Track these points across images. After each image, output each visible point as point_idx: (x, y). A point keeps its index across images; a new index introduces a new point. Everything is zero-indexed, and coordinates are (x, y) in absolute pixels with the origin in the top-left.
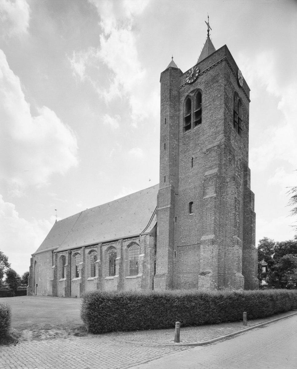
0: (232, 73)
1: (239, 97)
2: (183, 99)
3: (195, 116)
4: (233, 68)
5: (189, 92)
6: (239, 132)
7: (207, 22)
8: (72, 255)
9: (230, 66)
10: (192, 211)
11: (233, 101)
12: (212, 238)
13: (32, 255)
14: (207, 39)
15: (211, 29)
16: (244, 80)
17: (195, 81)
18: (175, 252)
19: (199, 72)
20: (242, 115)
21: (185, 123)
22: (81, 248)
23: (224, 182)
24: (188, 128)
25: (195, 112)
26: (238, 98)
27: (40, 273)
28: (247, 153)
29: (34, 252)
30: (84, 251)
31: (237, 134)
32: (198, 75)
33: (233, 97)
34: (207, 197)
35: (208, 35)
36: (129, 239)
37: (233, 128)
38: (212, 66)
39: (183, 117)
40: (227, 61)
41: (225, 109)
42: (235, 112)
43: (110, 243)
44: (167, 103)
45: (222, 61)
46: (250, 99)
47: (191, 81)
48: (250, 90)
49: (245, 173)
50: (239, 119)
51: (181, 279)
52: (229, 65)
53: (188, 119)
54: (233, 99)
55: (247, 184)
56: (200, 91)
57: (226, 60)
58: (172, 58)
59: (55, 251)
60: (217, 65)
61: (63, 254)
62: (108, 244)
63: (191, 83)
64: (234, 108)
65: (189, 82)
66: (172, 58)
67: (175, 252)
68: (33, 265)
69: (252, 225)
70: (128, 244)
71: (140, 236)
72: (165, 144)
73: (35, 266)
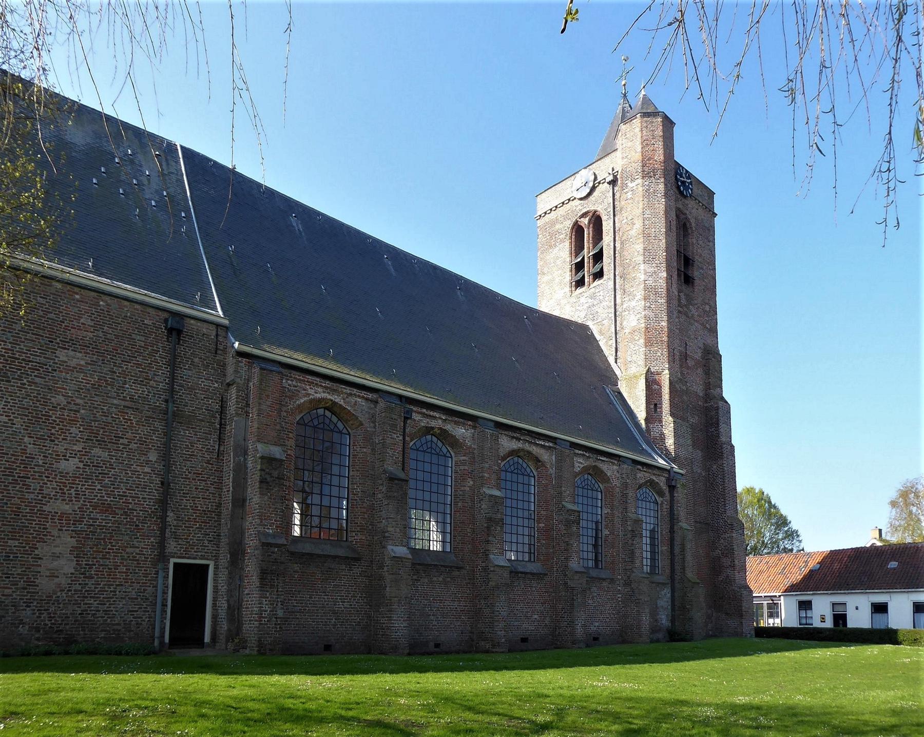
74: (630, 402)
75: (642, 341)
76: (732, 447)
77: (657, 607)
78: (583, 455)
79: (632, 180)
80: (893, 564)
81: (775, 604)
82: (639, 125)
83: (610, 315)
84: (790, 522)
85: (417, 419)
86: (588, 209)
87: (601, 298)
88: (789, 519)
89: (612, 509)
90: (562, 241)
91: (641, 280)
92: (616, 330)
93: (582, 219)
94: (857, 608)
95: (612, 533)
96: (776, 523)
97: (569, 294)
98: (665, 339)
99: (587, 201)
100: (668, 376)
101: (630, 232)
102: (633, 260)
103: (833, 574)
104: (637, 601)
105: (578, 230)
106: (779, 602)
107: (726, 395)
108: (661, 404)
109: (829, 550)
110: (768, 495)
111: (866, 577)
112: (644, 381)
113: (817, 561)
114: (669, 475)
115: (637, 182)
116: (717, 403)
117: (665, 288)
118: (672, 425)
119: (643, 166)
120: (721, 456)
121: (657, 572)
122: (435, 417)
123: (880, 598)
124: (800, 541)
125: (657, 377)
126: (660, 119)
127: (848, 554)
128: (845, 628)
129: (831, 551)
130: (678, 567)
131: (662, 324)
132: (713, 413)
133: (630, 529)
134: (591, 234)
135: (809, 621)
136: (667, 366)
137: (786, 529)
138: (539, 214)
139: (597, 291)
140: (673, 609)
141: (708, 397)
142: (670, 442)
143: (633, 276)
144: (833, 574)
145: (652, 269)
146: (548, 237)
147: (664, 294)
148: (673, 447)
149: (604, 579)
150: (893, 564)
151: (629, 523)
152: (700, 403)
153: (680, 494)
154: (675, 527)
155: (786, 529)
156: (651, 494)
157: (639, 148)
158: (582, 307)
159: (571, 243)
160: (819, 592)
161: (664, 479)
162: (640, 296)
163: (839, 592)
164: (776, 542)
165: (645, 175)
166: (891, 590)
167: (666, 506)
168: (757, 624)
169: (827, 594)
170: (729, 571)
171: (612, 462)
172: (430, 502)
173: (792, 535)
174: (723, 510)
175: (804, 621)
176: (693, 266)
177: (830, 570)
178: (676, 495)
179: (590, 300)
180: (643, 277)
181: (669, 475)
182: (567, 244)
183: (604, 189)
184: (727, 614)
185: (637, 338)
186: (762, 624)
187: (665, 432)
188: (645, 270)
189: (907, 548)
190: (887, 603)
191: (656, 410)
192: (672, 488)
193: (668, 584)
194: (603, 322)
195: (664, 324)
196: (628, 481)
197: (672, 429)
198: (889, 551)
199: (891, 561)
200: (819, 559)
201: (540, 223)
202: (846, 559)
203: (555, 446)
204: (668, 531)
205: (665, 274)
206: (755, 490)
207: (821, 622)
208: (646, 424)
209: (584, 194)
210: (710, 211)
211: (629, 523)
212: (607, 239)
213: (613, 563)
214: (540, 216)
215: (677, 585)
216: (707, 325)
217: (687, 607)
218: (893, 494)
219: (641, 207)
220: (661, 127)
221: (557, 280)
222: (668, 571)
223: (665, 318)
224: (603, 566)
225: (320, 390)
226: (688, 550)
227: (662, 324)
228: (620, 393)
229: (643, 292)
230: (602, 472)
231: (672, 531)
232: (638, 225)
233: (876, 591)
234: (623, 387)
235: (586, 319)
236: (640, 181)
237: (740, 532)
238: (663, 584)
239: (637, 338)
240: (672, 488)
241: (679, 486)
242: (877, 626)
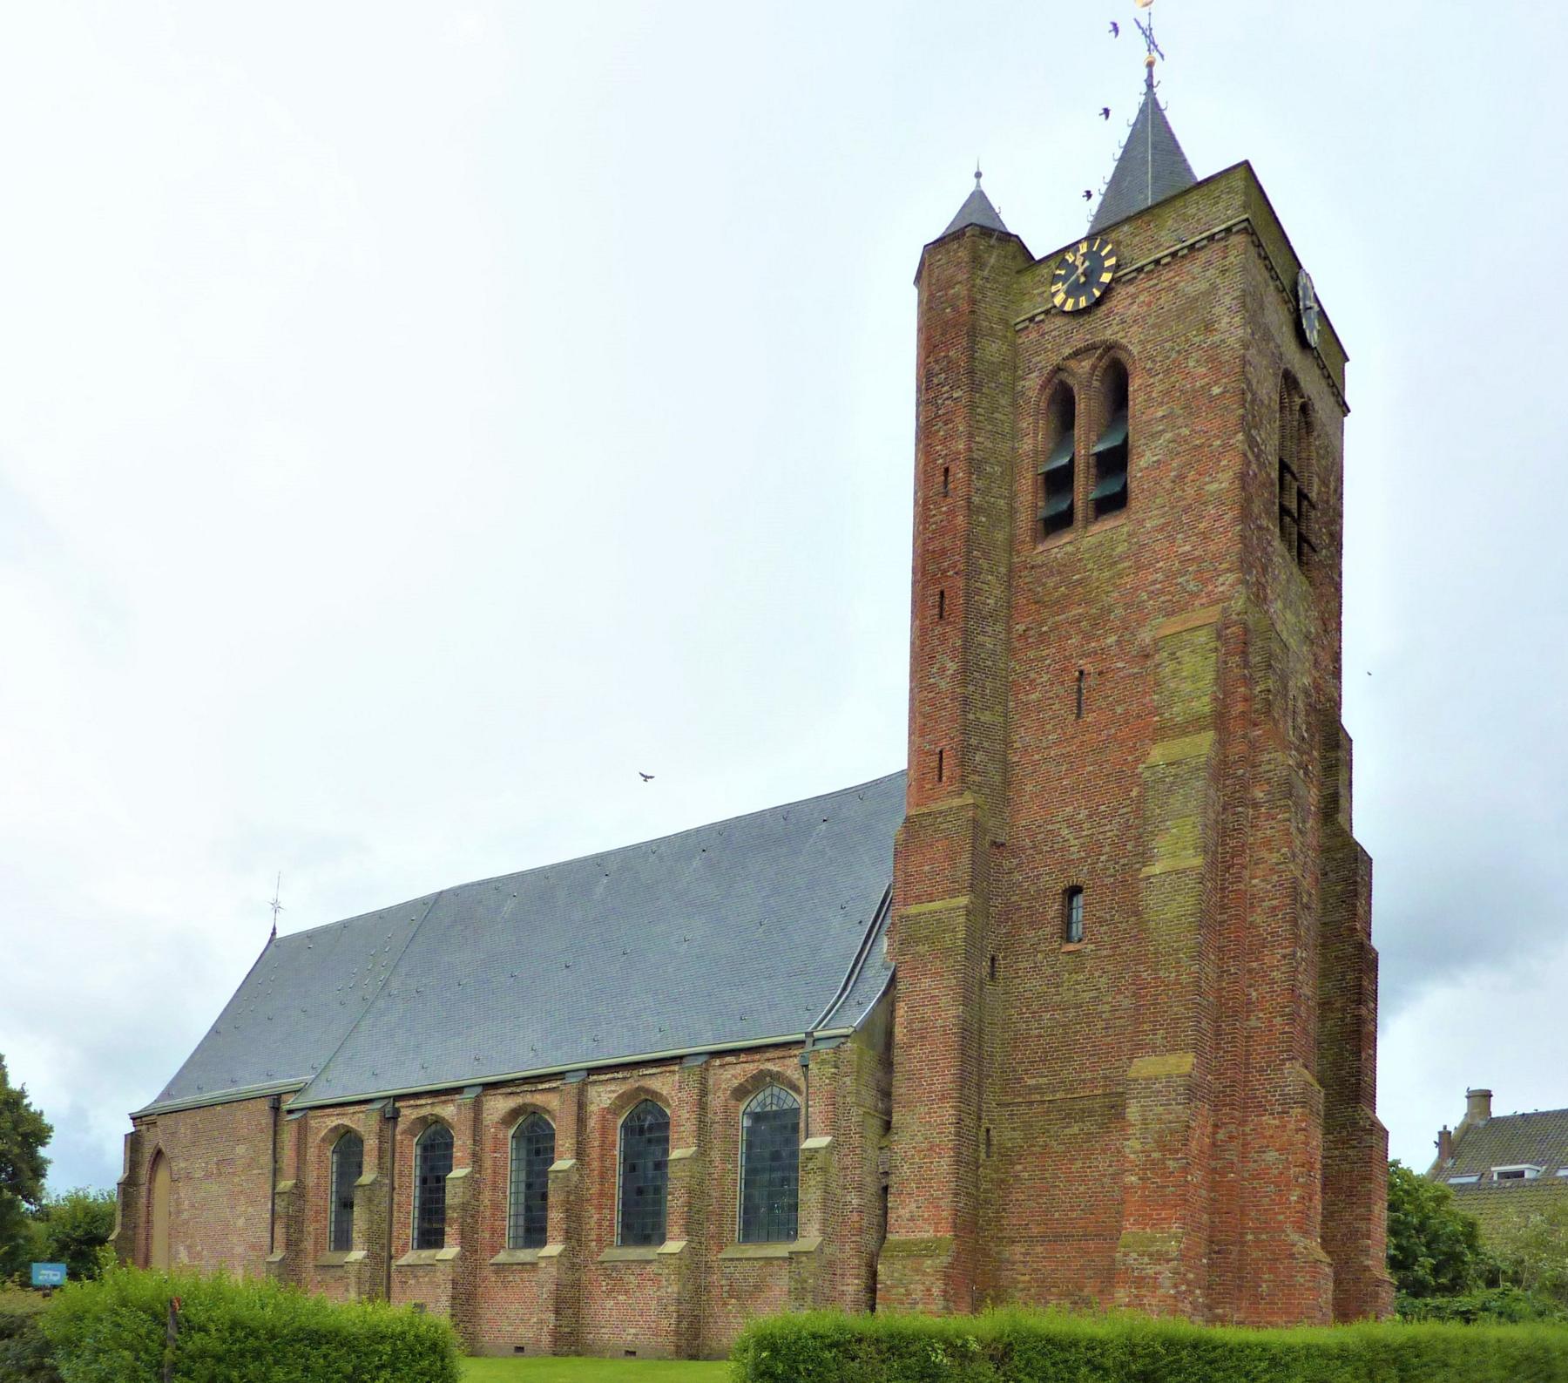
0: (1272, 288)
1: (1302, 397)
2: (1032, 384)
3: (1093, 471)
4: (1279, 262)
5: (1067, 351)
6: (1301, 561)
7: (1144, 24)
8: (401, 1127)
9: (1266, 258)
10: (1077, 930)
11: (1278, 415)
12: (1187, 1068)
13: (135, 1118)
14: (1142, 98)
15: (1162, 56)
16: (1322, 314)
17: (1099, 302)
18: (988, 1130)
19: (1118, 267)
20: (1315, 480)
21: (1041, 494)
22: (458, 1090)
23: (1242, 803)
24: (1058, 522)
25: (1099, 455)
26: (1298, 401)
27: (185, 1216)
28: (1337, 657)
29: (142, 1101)
30: (477, 1106)
31: (1295, 570)
32: (1113, 280)
33: (1276, 397)
34: (1157, 869)
35: (1150, 86)
36: (743, 1058)
37: (1277, 543)
38: (1182, 249)
39: (1035, 467)
40: (1253, 233)
41: (1245, 455)
42: (1284, 467)
43: (635, 1072)
44: (955, 395)
45: (1228, 230)
46: (1349, 398)
47: (1077, 303)
48: (1347, 359)
49: (1332, 755)
50: (1302, 496)
51: (1019, 1267)
52: (1263, 254)
53: (1058, 481)
54: (1277, 407)
55: (1336, 810)
56: (1122, 356)
57: (1249, 230)
58: (978, 175)
59: (289, 1103)
60: (1205, 246)
61: (346, 1121)
62: (620, 1075)
63: (1077, 313)
64: (1282, 446)
65: (1068, 307)
66: (978, 175)
67: (988, 1130)
68: (144, 1172)
69: (1364, 1011)
70: (736, 1083)
71: (809, 1041)
72: (942, 593)
73: (152, 1180)
85: (407, 1113)
122: (422, 1105)
171: (670, 1072)
206: (44, 1144)
225: (334, 1118)
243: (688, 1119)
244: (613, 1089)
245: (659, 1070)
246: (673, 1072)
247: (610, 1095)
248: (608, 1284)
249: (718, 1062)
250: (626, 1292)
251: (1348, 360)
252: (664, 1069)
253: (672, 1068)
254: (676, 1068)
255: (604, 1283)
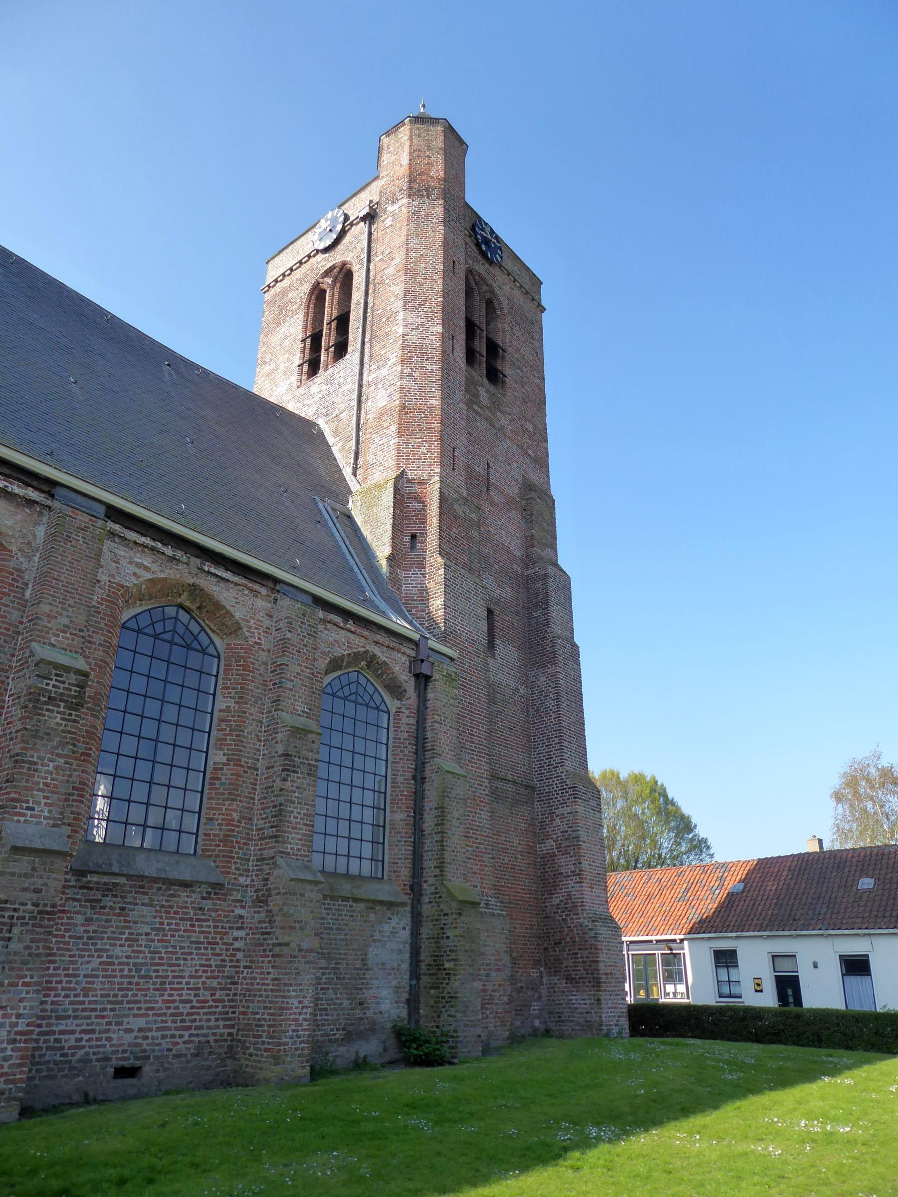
36: (350, 625)
62: (169, 551)
74: (366, 532)
75: (394, 428)
76: (575, 648)
77: (365, 967)
78: (153, 549)
79: (393, 202)
80: (866, 883)
81: (675, 954)
82: (408, 132)
83: (352, 404)
84: (695, 826)
86: (334, 262)
87: (341, 380)
88: (694, 820)
89: (241, 700)
90: (294, 313)
91: (398, 335)
92: (358, 424)
93: (325, 279)
94: (815, 966)
95: (234, 760)
96: (677, 827)
97: (295, 384)
98: (437, 426)
99: (331, 254)
100: (438, 486)
101: (386, 272)
102: (388, 309)
103: (767, 900)
104: (277, 950)
105: (318, 294)
106: (682, 952)
107: (563, 561)
108: (424, 534)
109: (756, 857)
110: (662, 785)
111: (824, 906)
112: (392, 490)
113: (739, 877)
114: (417, 652)
115: (400, 203)
116: (545, 569)
117: (439, 349)
118: (442, 571)
119: (410, 182)
120: (553, 658)
121: (380, 876)
123: (855, 946)
124: (712, 856)
125: (418, 488)
126: (440, 128)
127: (789, 864)
128: (798, 1009)
129: (759, 860)
130: (429, 864)
131: (431, 402)
132: (538, 585)
133: (280, 749)
134: (336, 296)
135: (735, 990)
136: (438, 470)
137: (690, 836)
138: (268, 283)
139: (335, 372)
140: (415, 973)
141: (529, 560)
142: (437, 603)
143: (387, 331)
144: (767, 900)
145: (417, 320)
146: (277, 312)
147: (437, 355)
148: (441, 612)
149: (185, 885)
150: (866, 883)
151: (279, 736)
152: (515, 567)
153: (438, 693)
154: (428, 766)
155: (690, 836)
156: (370, 689)
157: (405, 160)
158: (313, 400)
159: (307, 314)
160: (747, 934)
161: (404, 659)
162: (395, 359)
163: (781, 933)
164: (678, 856)
165: (412, 193)
166: (872, 931)
167: (407, 721)
168: (648, 994)
169: (762, 936)
170: (571, 884)
171: (251, 590)
172: (349, 838)
173: (700, 846)
174: (558, 760)
175: (725, 990)
176: (503, 358)
177: (761, 893)
178: (430, 695)
179: (324, 387)
180: (400, 330)
181: (417, 652)
182: (301, 316)
183: (359, 231)
184: (569, 979)
185: (386, 425)
186: (655, 993)
187: (429, 586)
188: (404, 320)
189: (883, 854)
190: (867, 956)
191: (413, 547)
192: (423, 680)
193: (403, 904)
194: (341, 416)
195: (436, 402)
196: (289, 635)
197: (441, 579)
198: (855, 859)
199: (861, 877)
200: (742, 874)
201: (267, 296)
202: (785, 873)
203: (49, 503)
204: (409, 775)
205: (439, 329)
207: (756, 991)
208: (390, 566)
209: (328, 242)
210: (533, 299)
211: (280, 736)
212: (357, 296)
213: (226, 839)
214: (269, 286)
215: (427, 910)
216: (530, 452)
217: (447, 965)
218: (835, 781)
219: (405, 233)
220: (442, 138)
221: (282, 367)
222: (405, 873)
223: (438, 394)
224: (199, 847)
226: (455, 822)
227: (431, 402)
228: (349, 517)
229: (400, 352)
230: (218, 606)
231: (419, 777)
232: (399, 258)
233: (846, 932)
234: (355, 508)
235: (316, 416)
236: (405, 201)
237: (593, 803)
238: (390, 905)
239: (386, 425)
240: (423, 680)
241: (436, 676)
242: (859, 1006)
243: (299, 674)
244: (145, 563)
245: (236, 579)
246: (256, 593)
247: (140, 572)
248: (89, 920)
249: (321, 614)
250: (132, 940)
251: (542, 283)
252: (244, 581)
253: (257, 587)
254: (264, 591)
255: (79, 919)
